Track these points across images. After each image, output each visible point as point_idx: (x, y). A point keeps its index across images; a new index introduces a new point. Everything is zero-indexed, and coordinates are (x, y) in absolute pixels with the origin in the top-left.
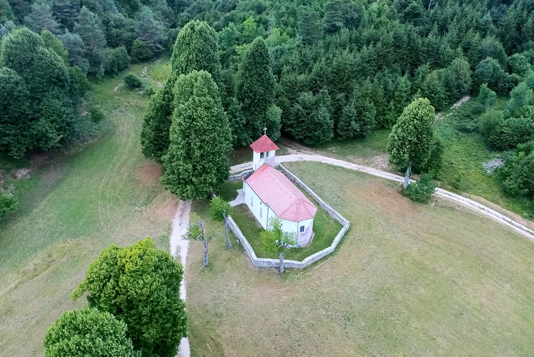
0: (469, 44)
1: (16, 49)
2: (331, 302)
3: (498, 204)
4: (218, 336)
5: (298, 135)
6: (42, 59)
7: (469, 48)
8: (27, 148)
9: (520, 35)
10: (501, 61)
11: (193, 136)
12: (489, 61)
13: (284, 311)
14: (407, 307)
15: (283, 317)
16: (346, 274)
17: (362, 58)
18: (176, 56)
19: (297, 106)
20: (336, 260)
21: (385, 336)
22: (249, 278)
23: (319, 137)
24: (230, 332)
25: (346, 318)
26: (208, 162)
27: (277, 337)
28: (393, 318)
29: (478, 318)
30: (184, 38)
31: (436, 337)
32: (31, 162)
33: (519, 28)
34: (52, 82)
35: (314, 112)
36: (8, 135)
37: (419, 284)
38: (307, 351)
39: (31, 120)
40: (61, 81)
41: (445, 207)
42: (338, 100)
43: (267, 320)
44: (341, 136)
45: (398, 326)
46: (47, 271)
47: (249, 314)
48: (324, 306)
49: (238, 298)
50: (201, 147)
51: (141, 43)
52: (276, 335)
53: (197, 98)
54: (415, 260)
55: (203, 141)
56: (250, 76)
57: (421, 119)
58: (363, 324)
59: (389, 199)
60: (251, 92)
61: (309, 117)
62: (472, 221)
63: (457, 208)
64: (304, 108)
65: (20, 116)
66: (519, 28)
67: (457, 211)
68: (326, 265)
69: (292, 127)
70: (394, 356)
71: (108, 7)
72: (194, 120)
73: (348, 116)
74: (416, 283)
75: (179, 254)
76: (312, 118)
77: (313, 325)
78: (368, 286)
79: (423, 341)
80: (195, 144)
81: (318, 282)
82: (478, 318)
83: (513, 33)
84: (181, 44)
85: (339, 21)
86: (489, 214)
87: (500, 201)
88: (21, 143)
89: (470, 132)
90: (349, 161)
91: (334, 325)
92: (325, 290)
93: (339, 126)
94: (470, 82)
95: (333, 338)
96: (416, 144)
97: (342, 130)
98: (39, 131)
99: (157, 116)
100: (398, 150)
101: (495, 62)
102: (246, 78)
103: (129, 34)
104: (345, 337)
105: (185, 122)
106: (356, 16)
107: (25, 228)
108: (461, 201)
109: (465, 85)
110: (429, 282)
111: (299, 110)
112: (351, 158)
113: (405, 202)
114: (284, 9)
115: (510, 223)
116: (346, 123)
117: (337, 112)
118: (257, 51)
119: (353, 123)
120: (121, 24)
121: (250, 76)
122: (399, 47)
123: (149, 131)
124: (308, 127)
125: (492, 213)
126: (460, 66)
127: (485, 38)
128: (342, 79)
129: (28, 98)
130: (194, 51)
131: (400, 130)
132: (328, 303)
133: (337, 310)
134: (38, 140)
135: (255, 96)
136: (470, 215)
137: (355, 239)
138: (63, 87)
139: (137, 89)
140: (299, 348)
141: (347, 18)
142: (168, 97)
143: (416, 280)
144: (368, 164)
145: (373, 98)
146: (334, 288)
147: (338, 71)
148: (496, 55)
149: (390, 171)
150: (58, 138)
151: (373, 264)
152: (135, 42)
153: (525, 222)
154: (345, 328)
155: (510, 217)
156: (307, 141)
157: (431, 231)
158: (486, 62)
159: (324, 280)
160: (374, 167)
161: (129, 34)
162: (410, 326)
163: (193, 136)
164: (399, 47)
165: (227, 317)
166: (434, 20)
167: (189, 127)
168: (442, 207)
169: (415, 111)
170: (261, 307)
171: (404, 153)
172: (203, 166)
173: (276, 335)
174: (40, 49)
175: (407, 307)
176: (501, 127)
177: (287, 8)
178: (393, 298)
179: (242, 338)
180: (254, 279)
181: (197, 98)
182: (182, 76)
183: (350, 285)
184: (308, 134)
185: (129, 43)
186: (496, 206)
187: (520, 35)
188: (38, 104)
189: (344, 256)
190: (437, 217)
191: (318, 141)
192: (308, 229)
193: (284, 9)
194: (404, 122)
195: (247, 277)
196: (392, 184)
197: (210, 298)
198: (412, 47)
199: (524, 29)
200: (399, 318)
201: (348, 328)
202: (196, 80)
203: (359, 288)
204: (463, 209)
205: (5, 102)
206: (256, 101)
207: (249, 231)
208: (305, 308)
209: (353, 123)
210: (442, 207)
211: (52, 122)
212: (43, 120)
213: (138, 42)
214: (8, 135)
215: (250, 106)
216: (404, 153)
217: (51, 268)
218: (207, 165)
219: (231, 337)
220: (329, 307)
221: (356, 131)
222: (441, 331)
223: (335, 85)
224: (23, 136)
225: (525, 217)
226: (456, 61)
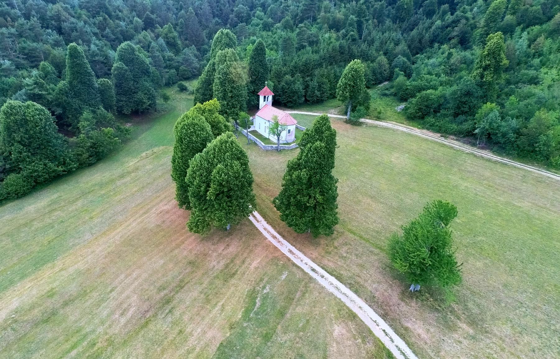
0: (387, 50)
1: (125, 52)
3: (403, 124)
5: (283, 100)
6: (138, 59)
7: (387, 53)
8: (132, 109)
9: (421, 45)
10: (409, 59)
11: (227, 84)
12: (400, 58)
14: (349, 162)
17: (320, 57)
18: (213, 50)
19: (283, 83)
23: (296, 100)
26: (235, 101)
30: (217, 38)
32: (133, 121)
33: (420, 42)
34: (144, 73)
35: (292, 86)
36: (122, 101)
39: (135, 93)
40: (148, 72)
41: (372, 126)
42: (306, 82)
44: (309, 101)
50: (231, 92)
51: (185, 68)
53: (228, 63)
55: (232, 87)
56: (255, 62)
57: (356, 71)
60: (256, 71)
61: (290, 89)
64: (286, 84)
65: (128, 90)
66: (420, 42)
67: (379, 127)
69: (280, 96)
71: (163, 49)
72: (227, 74)
73: (313, 88)
76: (292, 89)
80: (228, 89)
83: (416, 44)
84: (216, 42)
85: (305, 42)
87: (405, 122)
88: (128, 106)
89: (388, 96)
93: (308, 94)
94: (388, 71)
96: (354, 87)
97: (310, 96)
98: (138, 99)
99: (203, 87)
100: (343, 92)
101: (405, 59)
102: (253, 64)
103: (177, 64)
105: (223, 76)
106: (315, 39)
107: (136, 144)
109: (385, 72)
111: (283, 85)
113: (348, 126)
114: (270, 42)
116: (312, 92)
117: (307, 87)
118: (259, 47)
119: (316, 91)
120: (172, 58)
121: (255, 62)
122: (342, 53)
123: (199, 95)
124: (289, 95)
126: (381, 60)
128: (308, 70)
129: (132, 80)
130: (223, 44)
131: (344, 79)
134: (138, 105)
135: (258, 74)
136: (387, 129)
138: (149, 76)
139: (185, 91)
141: (310, 42)
142: (210, 74)
145: (328, 77)
147: (306, 64)
148: (404, 55)
149: (339, 115)
150: (149, 103)
152: (181, 68)
153: (419, 130)
155: (411, 129)
156: (289, 104)
158: (398, 59)
161: (177, 64)
163: (227, 84)
164: (342, 53)
166: (365, 41)
167: (225, 79)
168: (370, 127)
169: (352, 66)
171: (346, 93)
172: (233, 103)
174: (137, 53)
175: (349, 162)
176: (407, 86)
177: (272, 41)
181: (228, 63)
182: (220, 51)
184: (289, 100)
185: (177, 69)
187: (421, 45)
188: (137, 84)
191: (295, 104)
192: (292, 132)
193: (270, 42)
194: (346, 75)
196: (340, 119)
198: (351, 54)
199: (423, 41)
202: (228, 53)
205: (121, 82)
206: (259, 77)
209: (316, 91)
210: (370, 127)
211: (145, 94)
212: (140, 93)
213: (182, 68)
214: (122, 101)
215: (255, 80)
216: (346, 93)
218: (234, 103)
221: (317, 97)
223: (305, 73)
224: (129, 102)
225: (420, 128)
226: (379, 58)
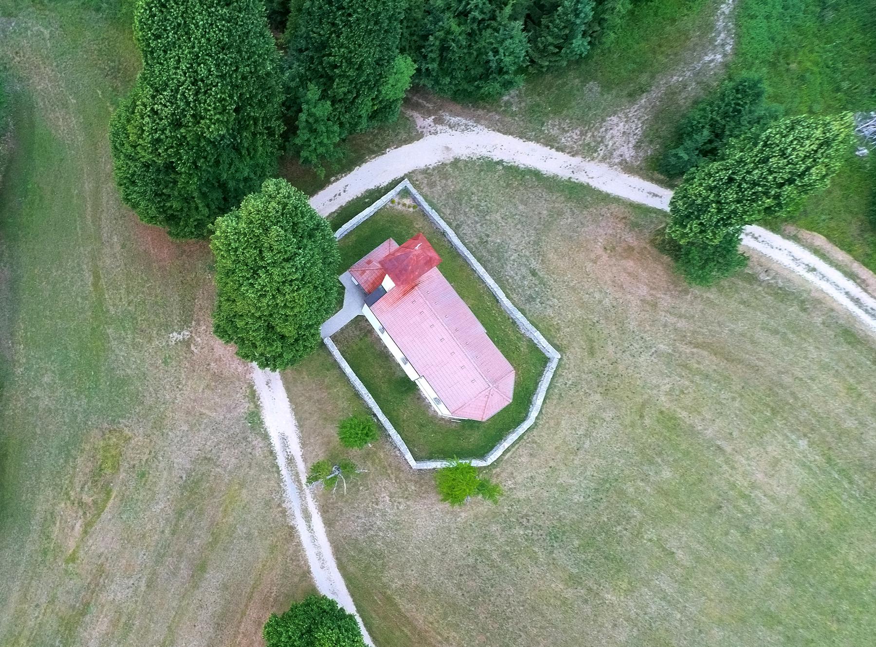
2: (531, 514)
4: (385, 586)
13: (466, 536)
15: (465, 546)
16: (552, 464)
20: (536, 439)
21: (605, 558)
22: (406, 485)
24: (400, 579)
25: (553, 537)
27: (462, 578)
28: (619, 528)
29: (742, 512)
31: (675, 551)
37: (663, 460)
38: (503, 593)
43: (444, 554)
45: (625, 539)
46: (111, 501)
47: (419, 548)
48: (521, 520)
49: (397, 523)
52: (461, 575)
54: (661, 412)
58: (576, 543)
59: (630, 264)
62: (783, 307)
63: (763, 277)
68: (520, 450)
70: (330, 3)
74: (659, 460)
75: (288, 450)
77: (508, 553)
78: (585, 478)
79: (657, 558)
81: (510, 482)
82: (742, 512)
86: (810, 276)
90: (550, 142)
91: (536, 549)
92: (521, 495)
95: (536, 570)
104: (552, 567)
108: (775, 255)
110: (680, 455)
112: (555, 132)
115: (857, 301)
125: (847, 293)
127: (289, 141)
132: (527, 515)
133: (540, 526)
137: (566, 384)
140: (492, 590)
143: (660, 454)
144: (588, 151)
146: (535, 490)
151: (594, 434)
154: (552, 552)
157: (700, 339)
159: (519, 479)
160: (604, 159)
162: (642, 537)
165: (391, 557)
170: (432, 535)
173: (461, 575)
178: (621, 493)
179: (417, 587)
180: (413, 488)
183: (558, 482)
186: (841, 256)
189: (549, 428)
190: (716, 301)
195: (403, 484)
197: (359, 528)
200: (628, 527)
201: (555, 552)
203: (571, 485)
204: (774, 278)
207: (385, 387)
208: (494, 528)
217: (114, 494)
219: (403, 586)
220: (528, 522)
222: (684, 539)
